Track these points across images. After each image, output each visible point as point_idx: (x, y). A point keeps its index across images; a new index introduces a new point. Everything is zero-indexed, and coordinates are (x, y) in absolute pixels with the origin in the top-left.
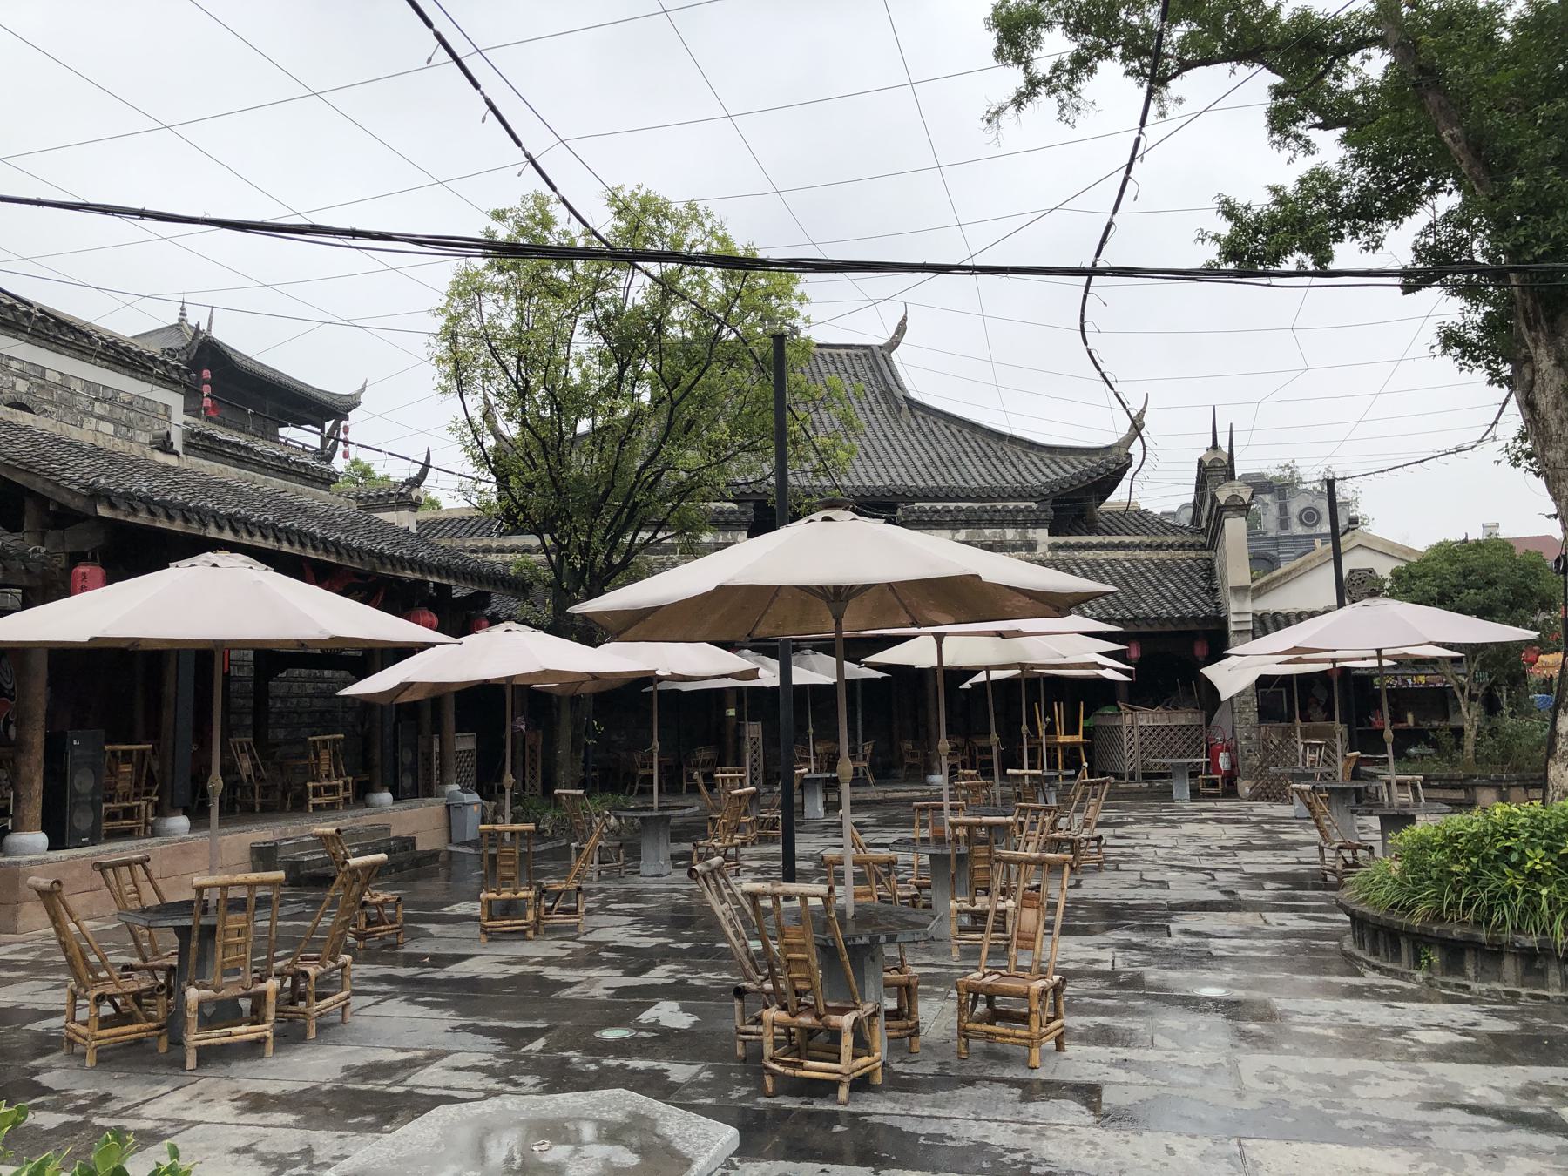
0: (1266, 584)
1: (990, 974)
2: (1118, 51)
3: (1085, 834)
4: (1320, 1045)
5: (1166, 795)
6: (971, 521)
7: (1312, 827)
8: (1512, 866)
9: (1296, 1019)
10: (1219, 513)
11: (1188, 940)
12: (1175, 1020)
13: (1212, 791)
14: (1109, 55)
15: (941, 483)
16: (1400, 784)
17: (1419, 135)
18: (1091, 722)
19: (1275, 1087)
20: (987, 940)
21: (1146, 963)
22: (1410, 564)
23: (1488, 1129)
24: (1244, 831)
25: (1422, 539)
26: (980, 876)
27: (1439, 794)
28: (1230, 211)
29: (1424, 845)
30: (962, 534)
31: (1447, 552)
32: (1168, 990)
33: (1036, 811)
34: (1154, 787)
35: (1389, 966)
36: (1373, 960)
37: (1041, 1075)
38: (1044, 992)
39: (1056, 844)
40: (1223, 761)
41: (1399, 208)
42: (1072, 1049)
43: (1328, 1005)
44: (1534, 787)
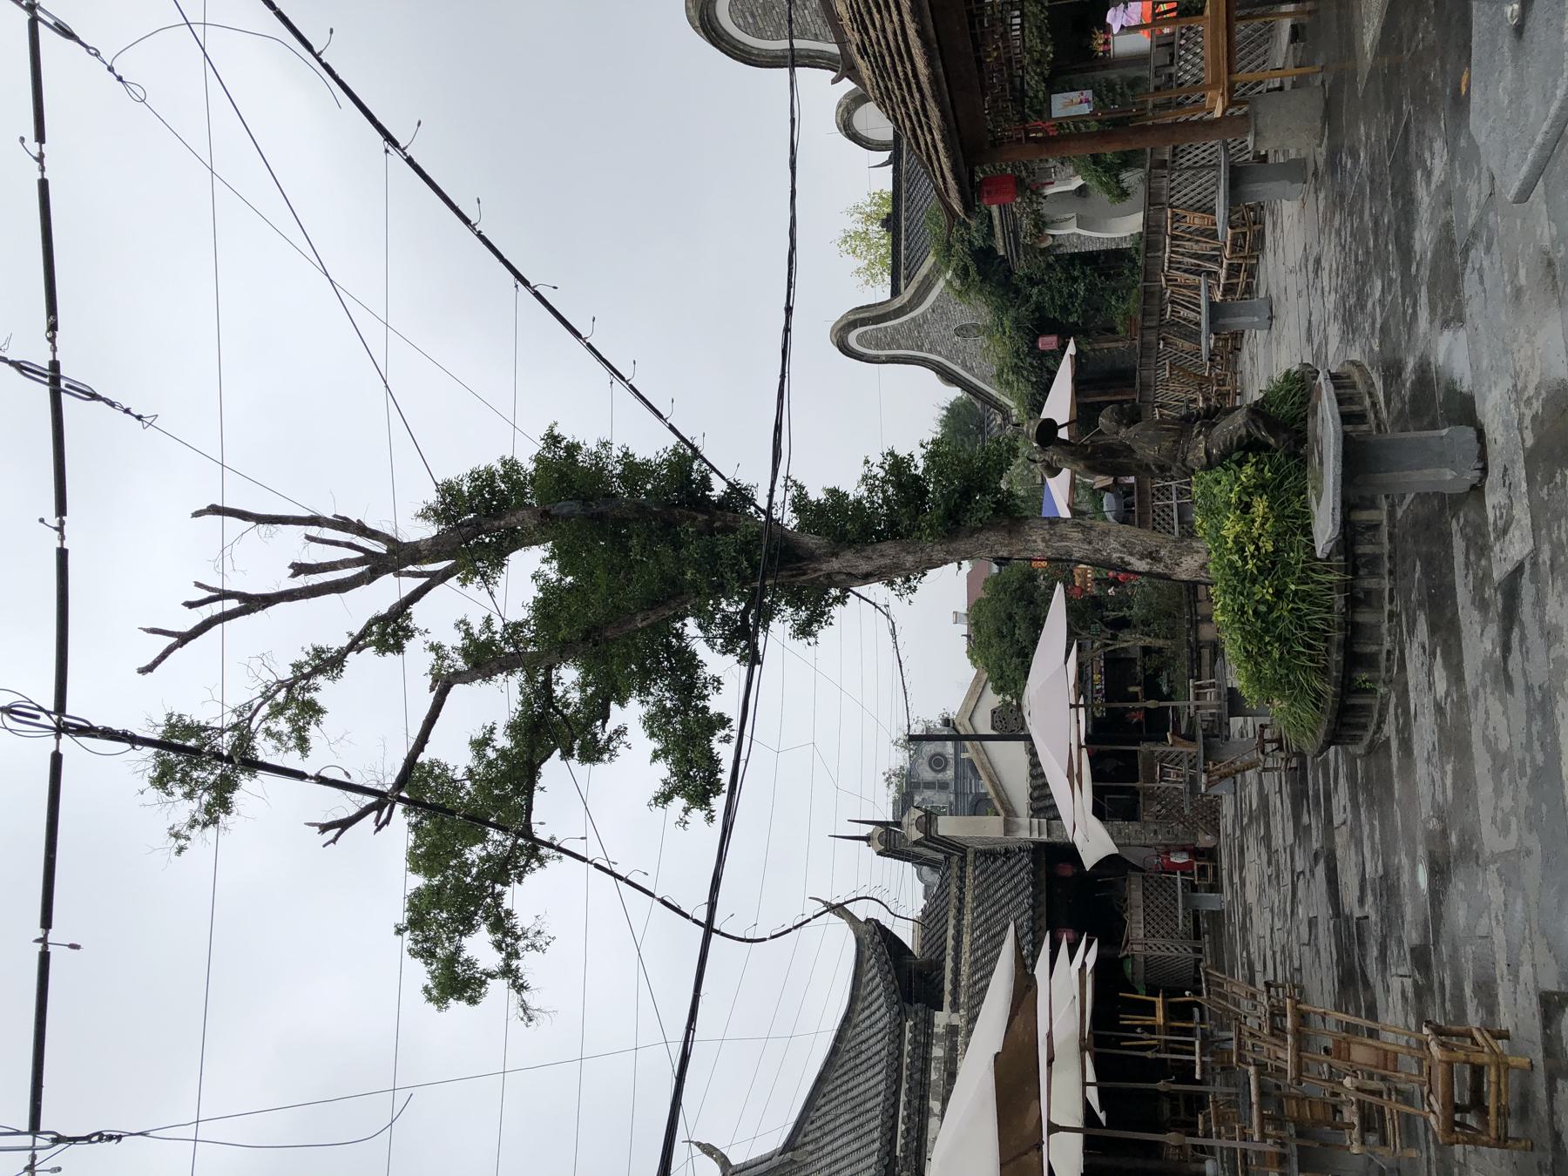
0: (1002, 803)
1: (1430, 1105)
2: (498, 888)
3: (1263, 999)
4: (1465, 783)
5: (1217, 917)
6: (921, 1092)
7: (1243, 776)
8: (1271, 610)
9: (1440, 798)
10: (931, 838)
11: (1370, 899)
12: (1458, 913)
13: (1210, 872)
14: (501, 894)
15: (878, 1122)
16: (1197, 697)
17: (635, 645)
18: (1141, 987)
19: (1514, 820)
20: (1392, 1107)
21: (1400, 942)
22: (990, 679)
23: (1523, 639)
24: (1251, 842)
25: (967, 672)
26: (1319, 1113)
27: (1206, 670)
28: (665, 798)
29: (1256, 678)
30: (935, 1105)
31: (978, 647)
32: (1426, 920)
33: (1240, 1046)
34: (1208, 929)
35: (1376, 716)
36: (1372, 728)
37: (1538, 1057)
38: (1443, 1045)
39: (1277, 1032)
40: (1180, 859)
41: (689, 663)
42: (1505, 1021)
43: (1421, 769)
44: (1196, 594)
